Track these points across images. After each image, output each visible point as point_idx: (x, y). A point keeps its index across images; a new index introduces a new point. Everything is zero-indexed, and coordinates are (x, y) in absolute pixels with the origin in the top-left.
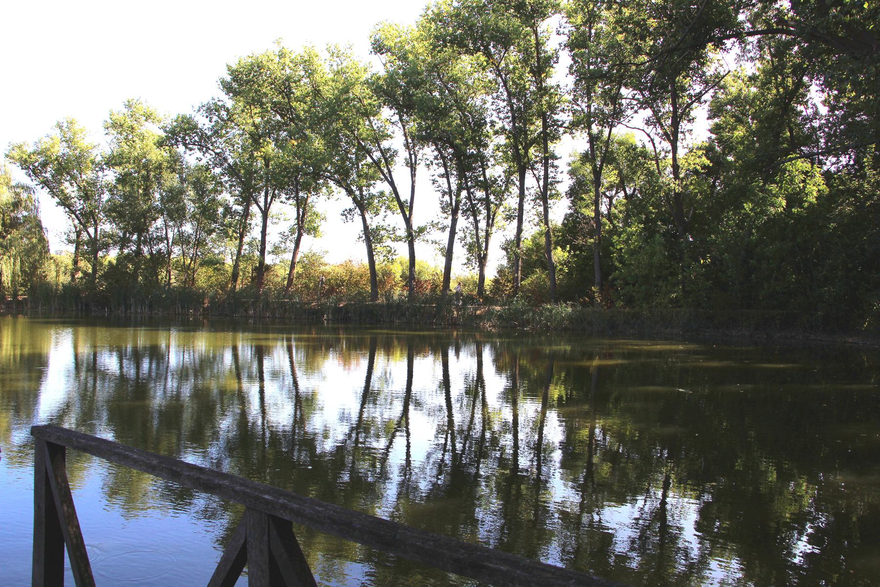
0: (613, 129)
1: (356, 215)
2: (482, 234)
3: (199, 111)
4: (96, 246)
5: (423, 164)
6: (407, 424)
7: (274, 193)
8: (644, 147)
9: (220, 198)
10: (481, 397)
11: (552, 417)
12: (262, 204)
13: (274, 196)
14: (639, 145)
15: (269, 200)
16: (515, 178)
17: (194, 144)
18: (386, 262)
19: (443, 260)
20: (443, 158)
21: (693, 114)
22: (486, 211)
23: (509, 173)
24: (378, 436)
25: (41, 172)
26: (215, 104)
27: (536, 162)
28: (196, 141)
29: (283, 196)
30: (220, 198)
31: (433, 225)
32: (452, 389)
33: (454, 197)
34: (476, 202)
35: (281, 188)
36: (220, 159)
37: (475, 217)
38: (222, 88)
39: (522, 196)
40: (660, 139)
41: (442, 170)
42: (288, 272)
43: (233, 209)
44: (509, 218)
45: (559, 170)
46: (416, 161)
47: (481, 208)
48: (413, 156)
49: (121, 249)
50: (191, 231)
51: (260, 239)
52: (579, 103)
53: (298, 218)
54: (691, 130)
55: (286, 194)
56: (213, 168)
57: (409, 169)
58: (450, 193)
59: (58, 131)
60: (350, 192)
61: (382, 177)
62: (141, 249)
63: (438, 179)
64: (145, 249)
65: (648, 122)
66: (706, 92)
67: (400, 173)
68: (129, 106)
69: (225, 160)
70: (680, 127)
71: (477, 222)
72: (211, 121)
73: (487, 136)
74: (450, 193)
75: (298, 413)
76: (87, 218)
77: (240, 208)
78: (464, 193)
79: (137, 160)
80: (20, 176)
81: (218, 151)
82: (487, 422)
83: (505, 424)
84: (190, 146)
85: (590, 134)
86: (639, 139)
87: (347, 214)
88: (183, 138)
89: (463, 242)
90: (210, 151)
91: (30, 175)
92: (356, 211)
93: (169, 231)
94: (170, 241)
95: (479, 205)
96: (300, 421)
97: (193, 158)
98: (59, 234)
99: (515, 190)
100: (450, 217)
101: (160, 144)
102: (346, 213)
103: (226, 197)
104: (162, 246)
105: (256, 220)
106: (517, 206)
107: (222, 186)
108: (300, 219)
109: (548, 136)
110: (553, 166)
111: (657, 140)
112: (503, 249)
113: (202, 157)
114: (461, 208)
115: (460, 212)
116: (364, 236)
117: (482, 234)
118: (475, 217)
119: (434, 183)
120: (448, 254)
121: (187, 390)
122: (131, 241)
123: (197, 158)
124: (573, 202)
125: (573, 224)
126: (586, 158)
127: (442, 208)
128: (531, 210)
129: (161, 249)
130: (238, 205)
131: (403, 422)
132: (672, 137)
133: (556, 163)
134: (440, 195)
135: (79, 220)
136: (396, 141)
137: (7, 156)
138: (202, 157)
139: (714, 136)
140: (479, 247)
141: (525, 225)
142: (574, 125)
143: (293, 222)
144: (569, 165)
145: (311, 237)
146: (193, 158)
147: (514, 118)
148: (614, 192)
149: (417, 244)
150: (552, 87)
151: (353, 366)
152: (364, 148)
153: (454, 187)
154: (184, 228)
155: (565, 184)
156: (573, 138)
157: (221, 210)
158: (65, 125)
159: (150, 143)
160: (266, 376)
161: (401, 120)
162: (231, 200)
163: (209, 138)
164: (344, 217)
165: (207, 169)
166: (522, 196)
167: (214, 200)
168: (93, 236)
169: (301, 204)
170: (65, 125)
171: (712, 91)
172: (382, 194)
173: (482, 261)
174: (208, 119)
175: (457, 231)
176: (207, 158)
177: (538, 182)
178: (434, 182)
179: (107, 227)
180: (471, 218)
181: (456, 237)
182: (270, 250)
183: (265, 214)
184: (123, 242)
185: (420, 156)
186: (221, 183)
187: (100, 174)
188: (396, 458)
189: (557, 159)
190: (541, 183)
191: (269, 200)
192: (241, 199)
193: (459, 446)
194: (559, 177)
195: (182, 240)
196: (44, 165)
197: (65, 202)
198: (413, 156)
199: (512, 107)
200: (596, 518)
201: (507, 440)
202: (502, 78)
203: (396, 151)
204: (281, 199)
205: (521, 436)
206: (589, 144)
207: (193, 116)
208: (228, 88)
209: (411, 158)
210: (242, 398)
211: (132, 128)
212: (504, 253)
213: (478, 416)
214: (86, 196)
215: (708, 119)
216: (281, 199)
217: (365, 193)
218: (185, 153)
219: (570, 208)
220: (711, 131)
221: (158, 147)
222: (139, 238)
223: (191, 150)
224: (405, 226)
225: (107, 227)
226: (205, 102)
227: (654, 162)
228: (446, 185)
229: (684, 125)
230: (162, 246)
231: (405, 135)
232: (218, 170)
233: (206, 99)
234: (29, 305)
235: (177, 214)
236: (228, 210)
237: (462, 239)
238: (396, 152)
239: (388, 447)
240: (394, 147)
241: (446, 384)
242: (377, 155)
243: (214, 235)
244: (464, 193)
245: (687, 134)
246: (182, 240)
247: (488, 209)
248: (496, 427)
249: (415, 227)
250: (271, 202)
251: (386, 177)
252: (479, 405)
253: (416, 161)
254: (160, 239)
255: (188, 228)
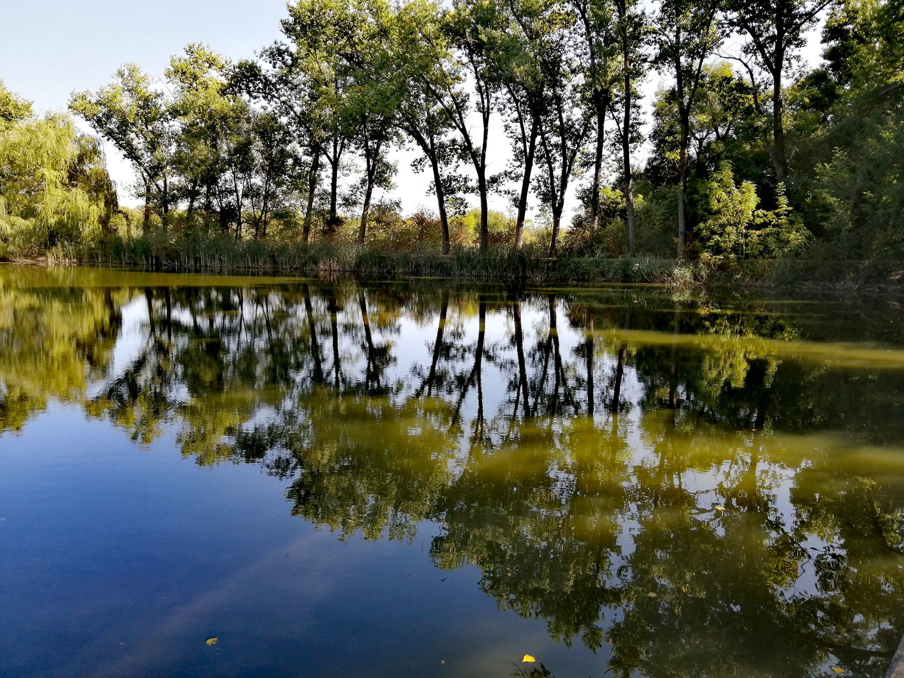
0: (705, 60)
1: (427, 165)
2: (557, 182)
3: (262, 56)
4: (166, 199)
5: (495, 110)
6: (479, 380)
7: (343, 143)
8: (741, 79)
9: (288, 148)
10: (554, 352)
11: (631, 374)
12: (331, 155)
13: (343, 146)
14: (736, 76)
15: (338, 150)
16: (594, 120)
17: (259, 92)
18: (457, 215)
19: (517, 210)
20: (516, 101)
21: (802, 36)
22: (562, 158)
23: (587, 118)
24: (450, 392)
25: (106, 124)
26: (278, 49)
27: (617, 102)
28: (259, 89)
29: (353, 147)
30: (288, 148)
31: (506, 174)
32: (524, 344)
33: (528, 144)
34: (551, 148)
35: (350, 138)
36: (287, 108)
37: (550, 163)
38: (284, 30)
39: (600, 140)
40: (760, 69)
41: (515, 115)
42: (359, 225)
43: (302, 160)
44: (586, 164)
45: (641, 111)
46: (488, 106)
47: (557, 155)
48: (486, 101)
49: (192, 202)
50: (260, 183)
51: (331, 191)
52: (666, 33)
53: (368, 169)
54: (799, 56)
55: (356, 144)
56: (280, 116)
57: (481, 115)
58: (524, 139)
59: (120, 80)
60: (421, 142)
61: (454, 124)
62: (210, 202)
63: (511, 124)
64: (215, 202)
65: (746, 50)
66: (821, 8)
67: (473, 120)
68: (190, 51)
69: (291, 107)
70: (785, 53)
71: (551, 170)
72: (274, 67)
73: (564, 76)
74: (524, 139)
75: (371, 365)
76: (155, 171)
77: (309, 159)
78: (538, 139)
79: (202, 113)
80: (85, 128)
81: (283, 99)
82: (561, 379)
83: (578, 380)
84: (255, 94)
85: (678, 67)
86: (737, 70)
87: (417, 165)
88: (247, 86)
89: (537, 192)
90: (275, 99)
91: (94, 127)
92: (426, 161)
93: (238, 183)
94: (240, 194)
95: (554, 151)
96: (373, 374)
97: (259, 106)
98: (128, 187)
99: (594, 134)
100: (524, 165)
101: (223, 92)
102: (416, 163)
103: (295, 147)
104: (232, 199)
105: (325, 175)
106: (594, 151)
107: (290, 135)
108: (370, 172)
109: (632, 74)
110: (635, 106)
111: (756, 70)
112: (579, 198)
113: (268, 105)
114: (535, 155)
115: (534, 159)
116: (435, 188)
117: (557, 182)
118: (550, 163)
119: (506, 130)
120: (521, 204)
121: (261, 343)
122: (200, 194)
123: (263, 107)
124: (657, 145)
125: (654, 171)
126: (673, 96)
127: (516, 156)
128: (611, 156)
129: (230, 203)
130: (308, 155)
131: (476, 377)
132: (775, 65)
133: (639, 102)
134: (512, 141)
135: (148, 173)
136: (468, 85)
137: (70, 107)
138: (268, 105)
139: (828, 62)
140: (554, 197)
141: (604, 171)
142: (661, 58)
143: (363, 174)
144: (655, 106)
145: (381, 189)
146: (259, 106)
147: (593, 54)
148: (705, 133)
149: (491, 196)
150: (637, 16)
151: (425, 320)
152: (434, 92)
153: (528, 133)
154: (253, 181)
155: (648, 125)
156: (659, 74)
157: (290, 161)
158: (127, 73)
159: (213, 90)
160: (340, 329)
161: (472, 61)
162: (300, 151)
163: (274, 85)
164: (414, 168)
165: (274, 119)
166: (600, 140)
167: (283, 151)
168: (162, 189)
169: (372, 155)
170: (127, 73)
171: (828, 6)
172: (454, 142)
173: (557, 212)
174: (271, 65)
175: (531, 180)
176: (272, 107)
177: (618, 124)
178: (507, 127)
179: (176, 180)
180: (546, 165)
181: (530, 187)
182: (341, 202)
183: (335, 164)
184: (193, 195)
185: (492, 101)
186: (289, 133)
187: (165, 124)
188: (469, 411)
189: (639, 98)
190: (622, 125)
191: (338, 150)
192: (310, 150)
193: (531, 401)
194: (642, 118)
195: (250, 192)
196: (109, 117)
197: (132, 154)
198: (486, 101)
199: (590, 41)
200: (676, 482)
201: (581, 395)
202: (580, 9)
203: (468, 95)
204: (351, 150)
205: (596, 392)
206: (676, 80)
207: (255, 61)
208: (289, 30)
209: (483, 102)
210: (316, 350)
211: (195, 76)
212: (580, 202)
213: (551, 371)
214: (153, 146)
215: (823, 42)
216: (351, 150)
217: (435, 141)
218: (249, 101)
219: (654, 151)
220: (825, 57)
221: (221, 96)
222: (208, 190)
223: (255, 98)
224: (477, 177)
225: (176, 180)
226: (267, 47)
227: (750, 96)
228: (520, 131)
229: (791, 51)
230: (232, 199)
231: (477, 77)
232: (284, 120)
233: (269, 44)
234: (100, 260)
235: (245, 167)
236: (297, 161)
237: (534, 189)
238: (468, 95)
239: (459, 403)
240: (466, 91)
241: (517, 339)
242: (448, 100)
243: (284, 188)
244: (538, 139)
245: (793, 61)
246: (250, 192)
247: (564, 155)
248: (571, 383)
249: (487, 177)
250: (340, 153)
251: (458, 126)
252: (551, 362)
253: (488, 106)
254: (231, 192)
255: (257, 180)
